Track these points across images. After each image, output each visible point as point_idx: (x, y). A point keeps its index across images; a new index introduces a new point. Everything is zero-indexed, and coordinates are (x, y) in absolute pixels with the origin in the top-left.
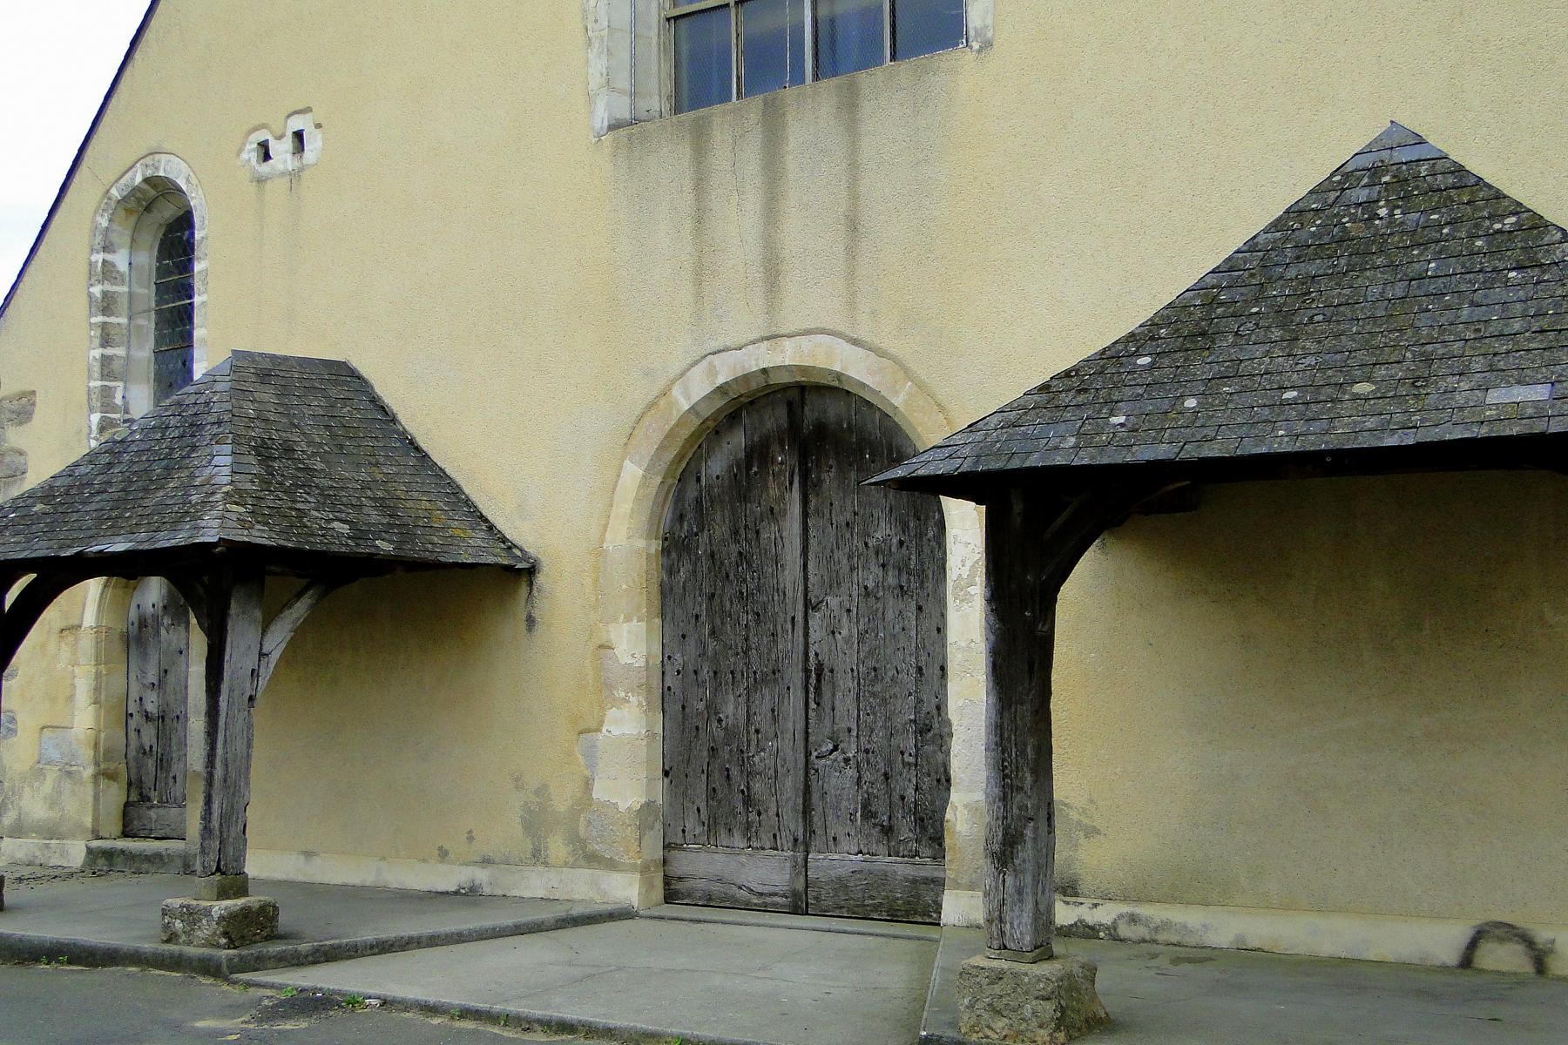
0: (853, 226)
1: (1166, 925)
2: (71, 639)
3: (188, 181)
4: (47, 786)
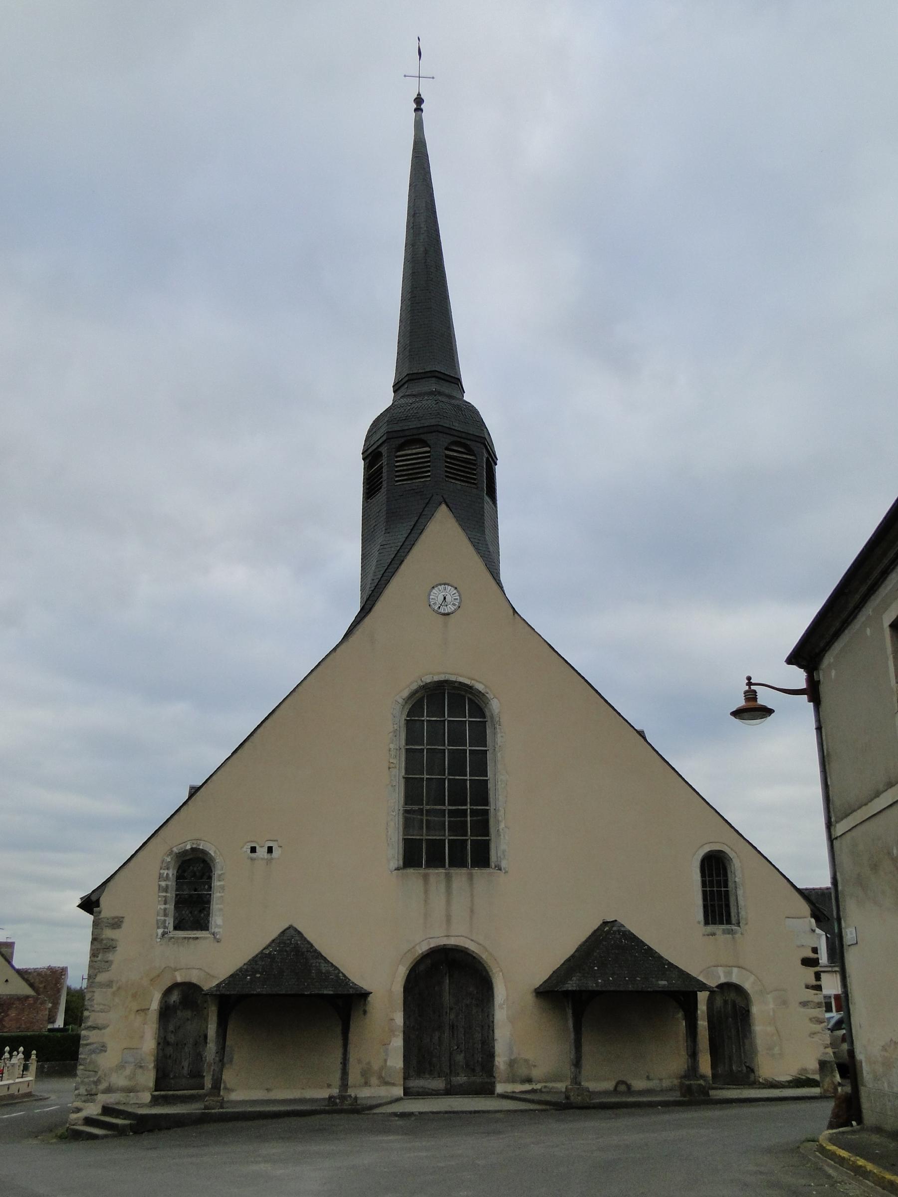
0: (472, 911)
1: (553, 1088)
2: (143, 1014)
3: (215, 852)
4: (128, 1072)
